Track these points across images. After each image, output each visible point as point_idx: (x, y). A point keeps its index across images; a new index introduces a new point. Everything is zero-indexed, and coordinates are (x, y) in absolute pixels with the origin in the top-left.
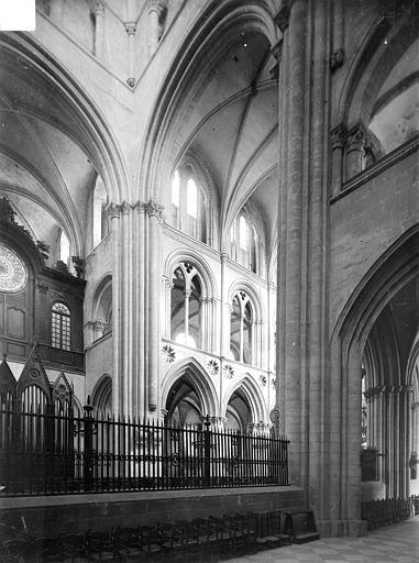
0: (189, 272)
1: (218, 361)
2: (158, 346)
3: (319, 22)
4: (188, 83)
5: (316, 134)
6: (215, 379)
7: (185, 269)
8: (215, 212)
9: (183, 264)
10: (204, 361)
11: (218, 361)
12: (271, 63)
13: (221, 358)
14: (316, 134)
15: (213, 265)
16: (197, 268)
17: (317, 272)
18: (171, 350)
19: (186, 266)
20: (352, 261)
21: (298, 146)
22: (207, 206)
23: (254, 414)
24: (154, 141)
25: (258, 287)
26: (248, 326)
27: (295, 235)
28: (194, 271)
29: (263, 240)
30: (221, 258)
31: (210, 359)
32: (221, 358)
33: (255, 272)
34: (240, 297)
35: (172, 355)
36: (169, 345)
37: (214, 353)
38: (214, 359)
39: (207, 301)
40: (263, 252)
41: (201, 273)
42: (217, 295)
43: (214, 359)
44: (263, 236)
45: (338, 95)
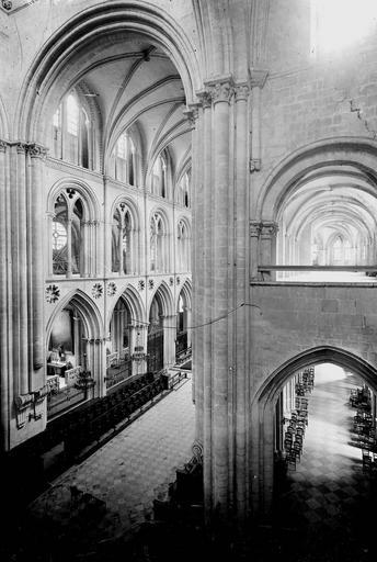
0: (71, 197)
1: (102, 283)
2: (42, 287)
3: (240, 118)
4: (78, 51)
5: (240, 227)
6: (99, 302)
8: (97, 133)
11: (102, 283)
12: (165, 391)
13: (105, 280)
14: (240, 227)
15: (96, 187)
16: (78, 191)
18: (54, 289)
19: (68, 191)
21: (224, 358)
22: (88, 127)
28: (77, 196)
29: (139, 152)
30: (104, 180)
31: (94, 283)
33: (132, 183)
34: (120, 209)
35: (57, 294)
36: (52, 284)
39: (90, 223)
42: (100, 217)
44: (139, 147)
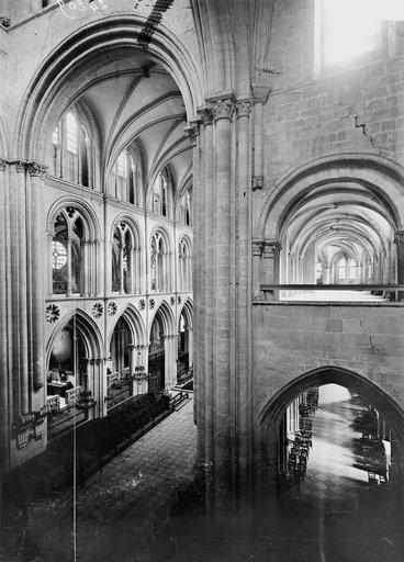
0: (71, 216)
2: (42, 306)
3: (243, 136)
6: (99, 322)
7: (67, 214)
9: (65, 210)
10: (89, 309)
11: (102, 302)
13: (105, 299)
14: (242, 246)
17: (245, 371)
20: (275, 366)
22: (88, 145)
23: (134, 337)
24: (38, 100)
25: (136, 216)
26: (128, 253)
27: (225, 335)
28: (76, 214)
30: (104, 198)
31: (95, 303)
32: (105, 299)
36: (52, 304)
37: (99, 296)
38: (98, 302)
40: (140, 182)
41: (84, 216)
42: (101, 236)
43: (98, 302)
45: (258, 214)
